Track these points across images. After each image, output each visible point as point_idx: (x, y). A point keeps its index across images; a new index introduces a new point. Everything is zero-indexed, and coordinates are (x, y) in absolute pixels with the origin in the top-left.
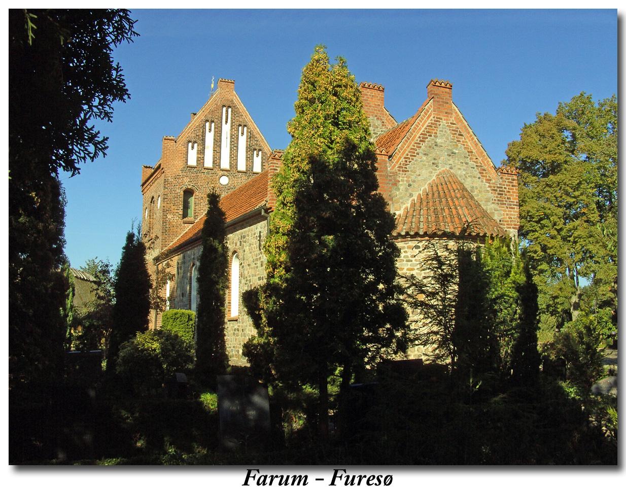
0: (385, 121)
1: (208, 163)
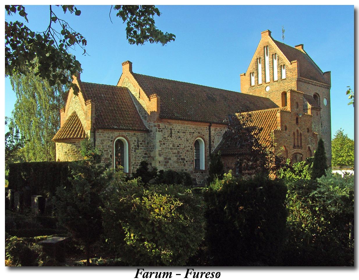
1: (260, 82)
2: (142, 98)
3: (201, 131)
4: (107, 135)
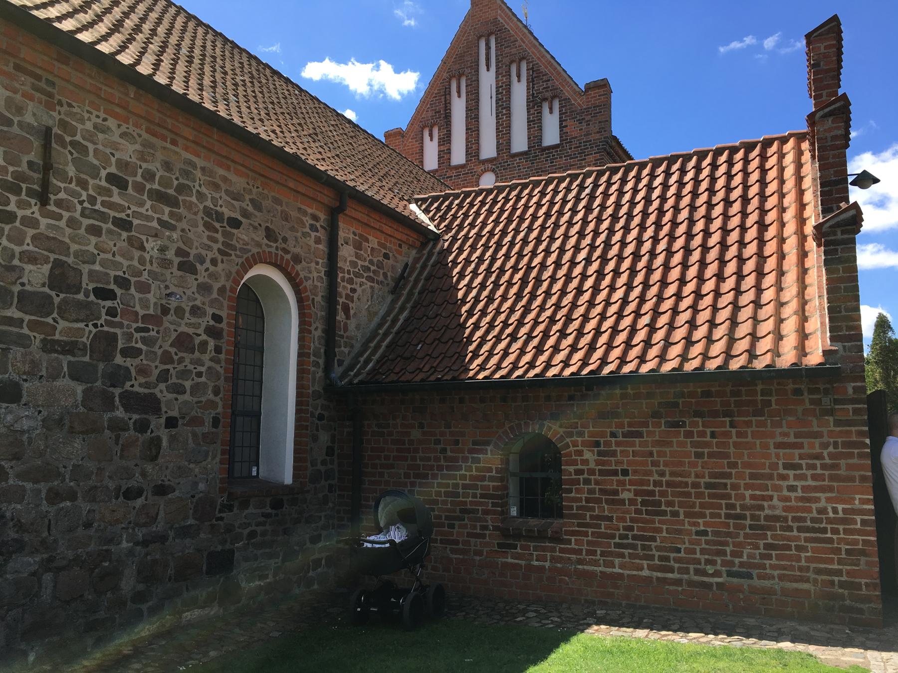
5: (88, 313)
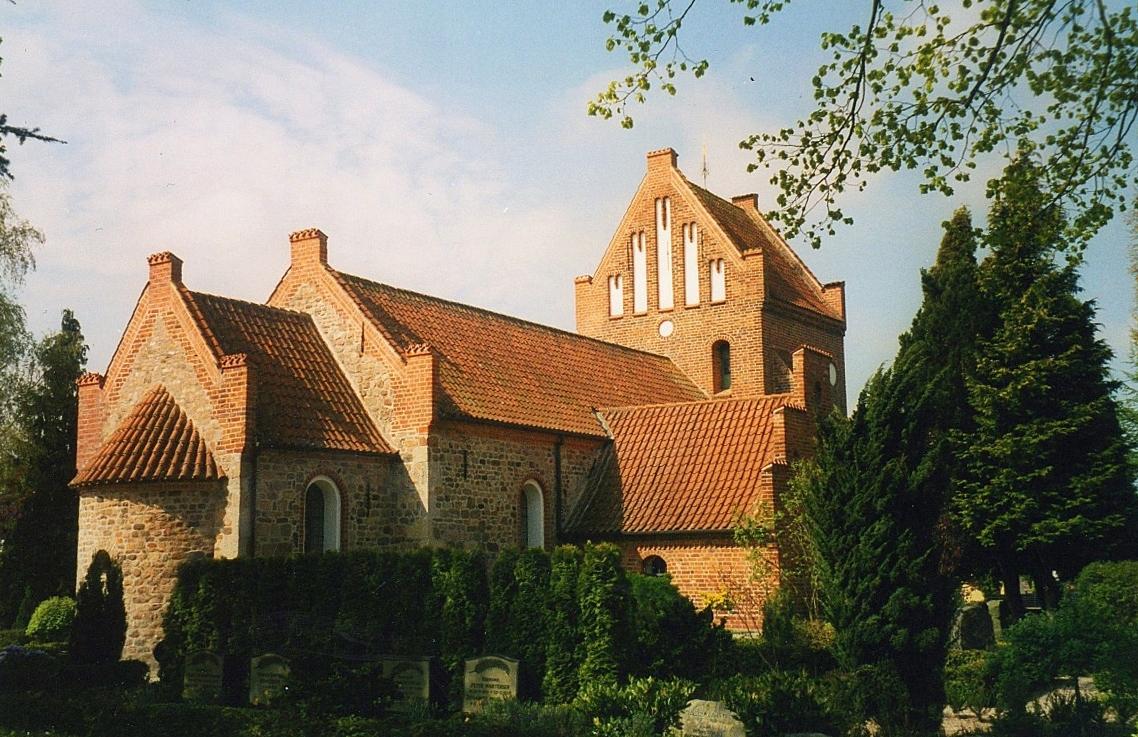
0: (321, 283)
1: (641, 306)
2: (374, 353)
3: (536, 461)
4: (286, 469)
5: (476, 514)
